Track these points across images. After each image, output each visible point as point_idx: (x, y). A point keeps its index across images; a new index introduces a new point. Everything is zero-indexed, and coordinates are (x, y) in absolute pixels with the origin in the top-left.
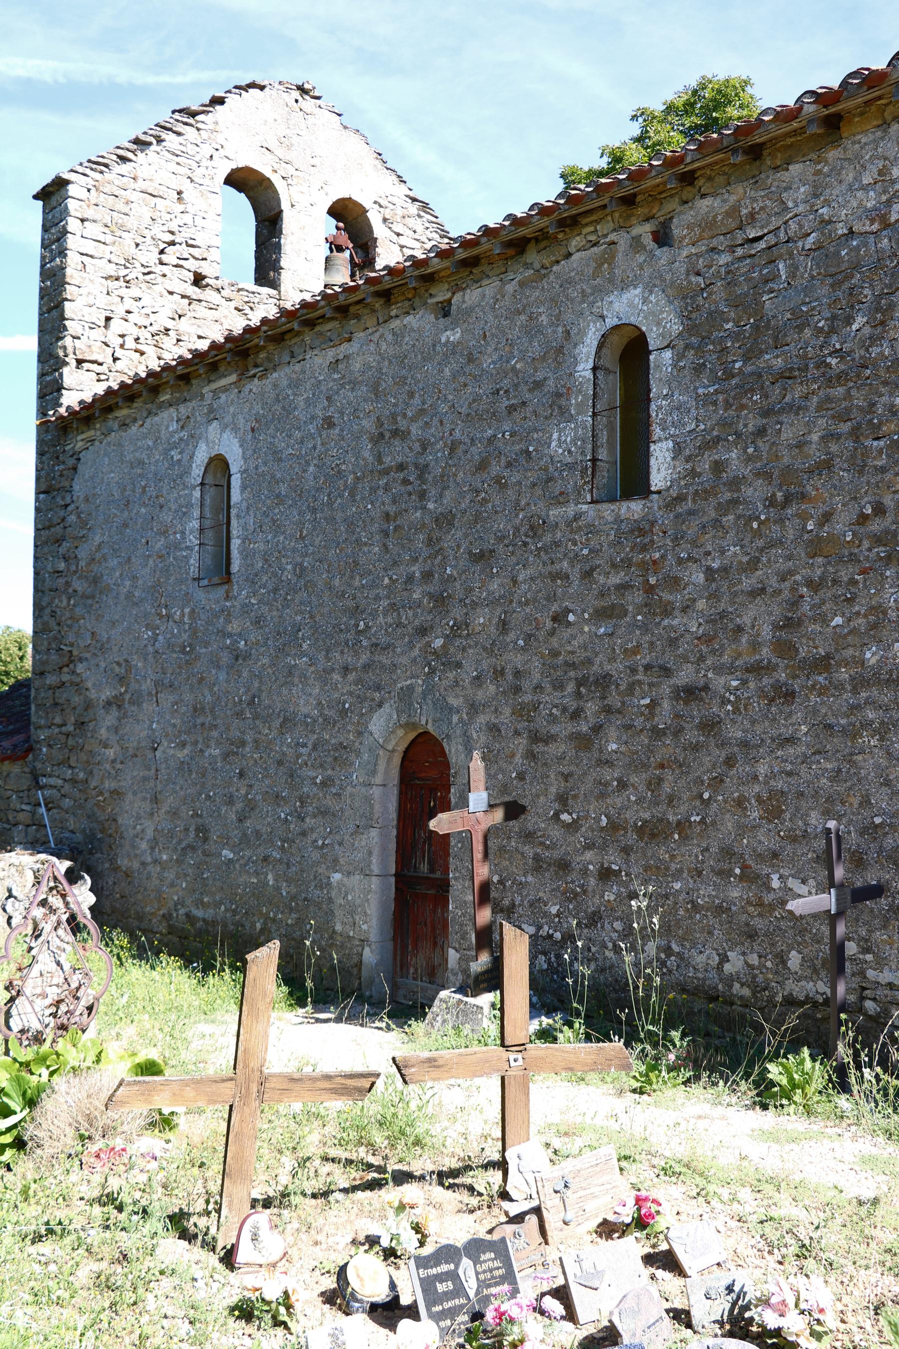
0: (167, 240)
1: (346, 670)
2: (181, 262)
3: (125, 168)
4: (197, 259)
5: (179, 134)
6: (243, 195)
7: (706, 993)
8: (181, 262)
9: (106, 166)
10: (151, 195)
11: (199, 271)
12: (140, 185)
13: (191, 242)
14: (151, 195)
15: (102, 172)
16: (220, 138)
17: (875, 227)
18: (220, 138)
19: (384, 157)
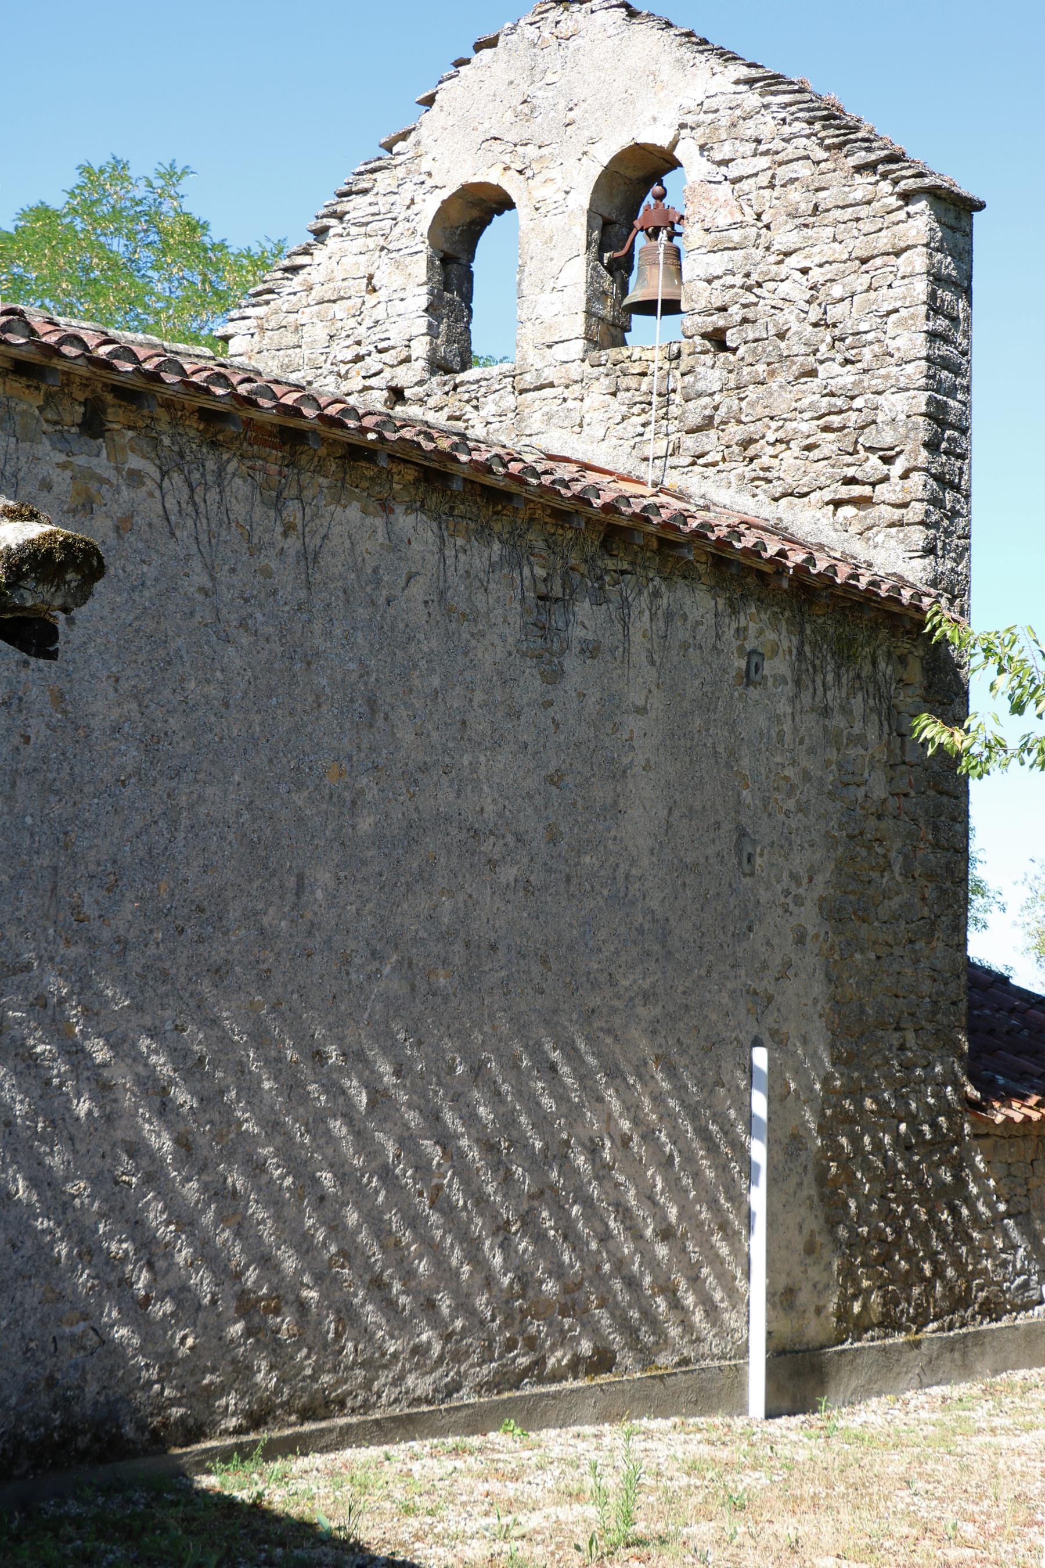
0: (350, 358)
1: (233, 570)
2: (369, 382)
3: (297, 282)
4: (392, 366)
5: (365, 192)
6: (475, 266)
7: (301, 1317)
8: (369, 382)
9: (270, 291)
10: (329, 301)
11: (393, 384)
12: (317, 293)
13: (381, 345)
14: (329, 301)
15: (267, 303)
16: (426, 165)
17: (914, 1532)
18: (426, 165)
19: (701, 34)
